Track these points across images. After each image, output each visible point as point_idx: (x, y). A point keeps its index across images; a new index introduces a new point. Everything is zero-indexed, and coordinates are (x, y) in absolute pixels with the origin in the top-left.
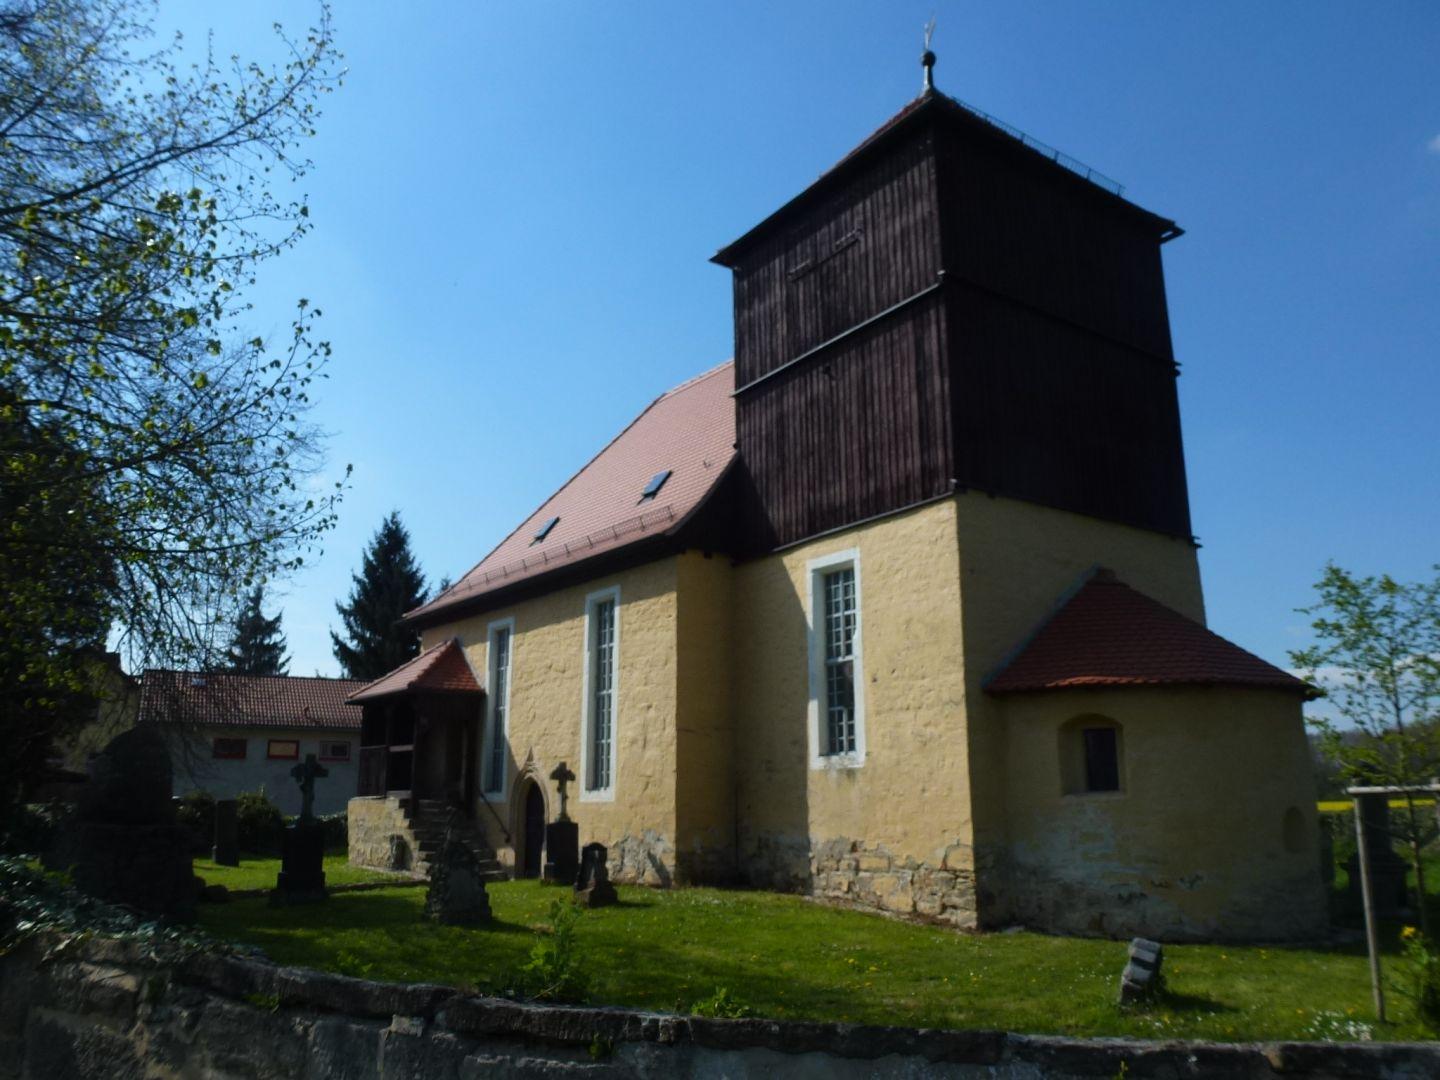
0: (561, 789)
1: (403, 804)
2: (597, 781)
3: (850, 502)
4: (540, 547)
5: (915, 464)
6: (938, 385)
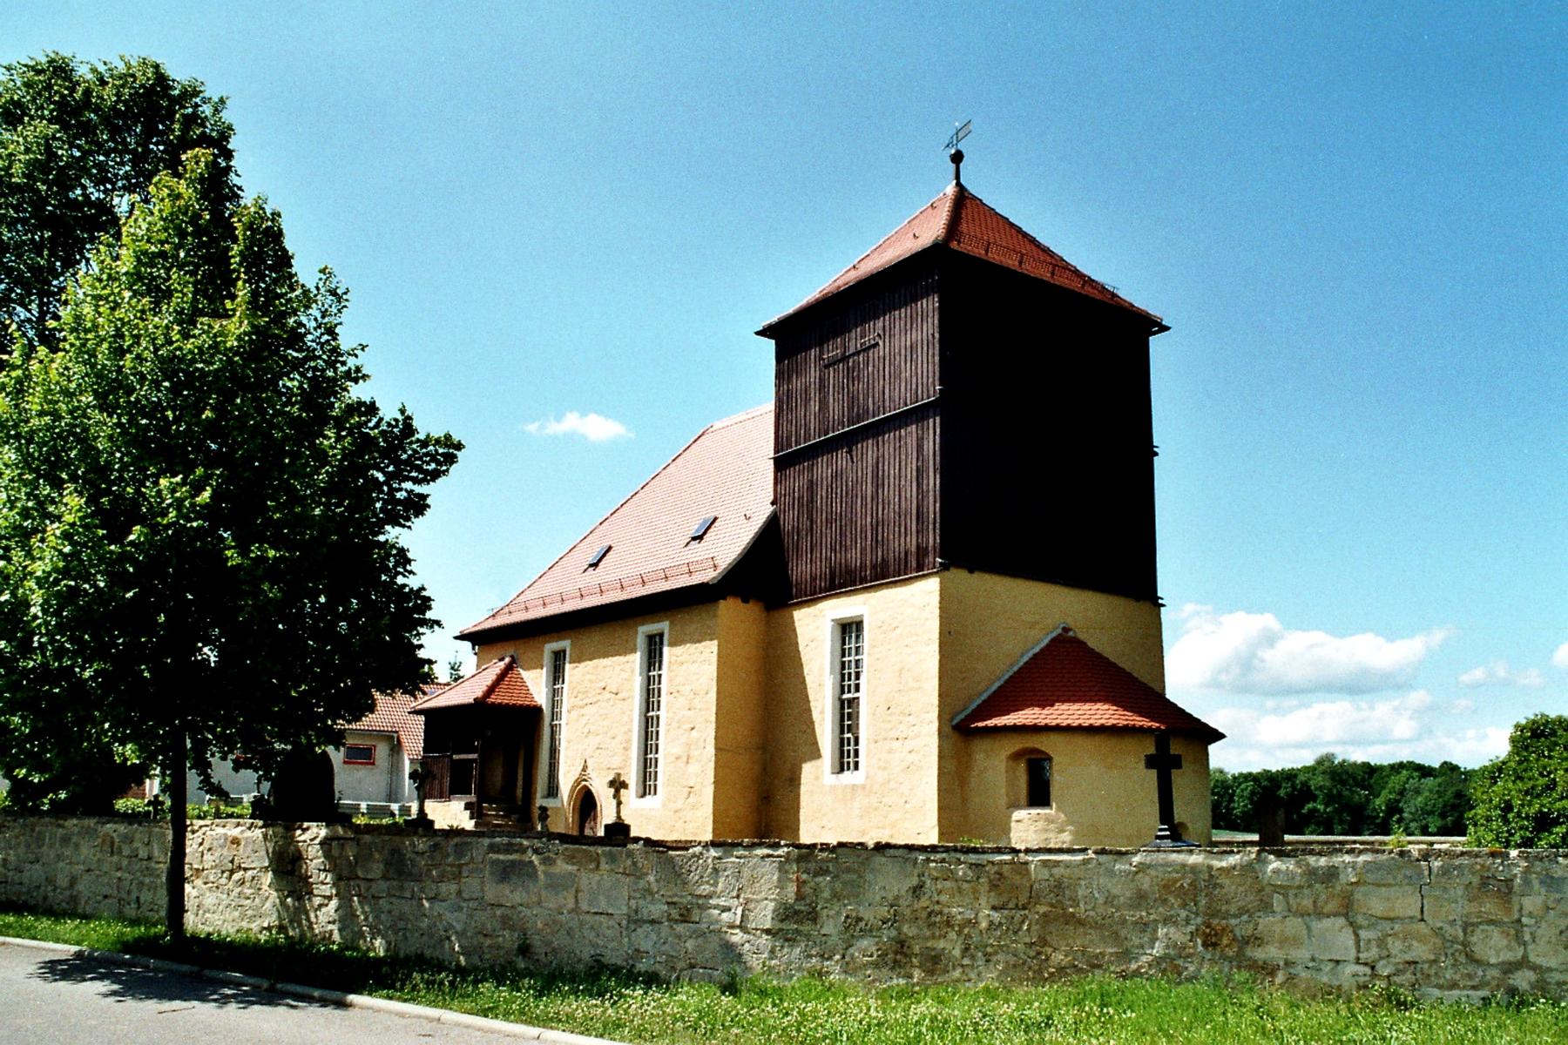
0: (617, 795)
1: (468, 806)
2: (646, 789)
3: (863, 567)
4: (595, 577)
5: (912, 543)
6: (933, 481)
